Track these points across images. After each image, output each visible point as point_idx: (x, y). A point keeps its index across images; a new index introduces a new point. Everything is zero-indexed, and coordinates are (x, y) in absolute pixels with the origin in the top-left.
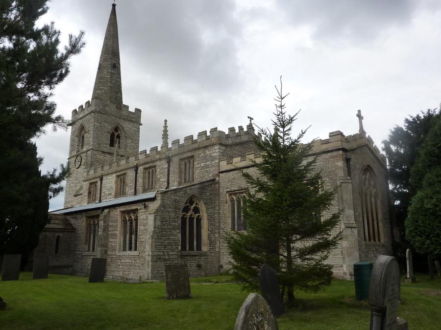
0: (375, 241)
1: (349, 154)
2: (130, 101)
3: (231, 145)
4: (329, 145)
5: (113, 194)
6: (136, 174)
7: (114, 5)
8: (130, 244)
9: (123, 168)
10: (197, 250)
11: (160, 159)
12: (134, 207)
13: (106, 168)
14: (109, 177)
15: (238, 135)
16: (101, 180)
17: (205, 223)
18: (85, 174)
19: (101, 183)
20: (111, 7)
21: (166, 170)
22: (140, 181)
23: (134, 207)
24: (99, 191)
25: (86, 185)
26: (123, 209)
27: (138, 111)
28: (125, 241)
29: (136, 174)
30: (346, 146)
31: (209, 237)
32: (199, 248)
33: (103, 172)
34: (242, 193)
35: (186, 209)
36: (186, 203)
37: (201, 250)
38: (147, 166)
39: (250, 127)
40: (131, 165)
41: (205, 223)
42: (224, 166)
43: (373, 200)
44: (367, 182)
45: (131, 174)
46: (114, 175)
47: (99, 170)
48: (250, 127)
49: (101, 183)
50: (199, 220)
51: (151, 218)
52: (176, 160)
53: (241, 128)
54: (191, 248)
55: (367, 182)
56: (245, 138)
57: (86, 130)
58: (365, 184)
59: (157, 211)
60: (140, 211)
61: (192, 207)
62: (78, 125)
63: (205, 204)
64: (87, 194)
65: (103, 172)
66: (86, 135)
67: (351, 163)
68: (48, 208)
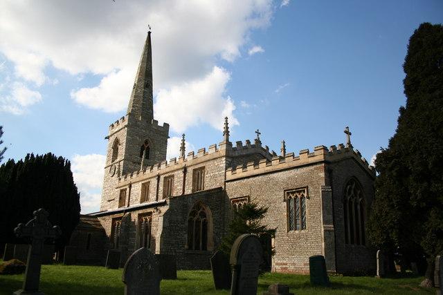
0: (358, 244)
1: (332, 166)
2: (161, 114)
3: (237, 157)
4: (315, 158)
5: (139, 199)
6: (158, 182)
7: (149, 33)
8: (146, 243)
9: (148, 177)
10: (203, 249)
11: (178, 170)
12: (149, 210)
13: (135, 176)
14: (136, 185)
15: (245, 148)
16: (130, 187)
17: (211, 228)
18: (117, 182)
19: (130, 189)
20: (147, 34)
21: (182, 179)
22: (161, 188)
23: (149, 210)
24: (127, 197)
25: (117, 192)
26: (141, 212)
27: (166, 126)
28: (141, 240)
29: (158, 182)
30: (329, 159)
31: (214, 239)
32: (205, 248)
33: (159, 171)
34: (243, 200)
35: (193, 214)
36: (194, 208)
37: (206, 250)
38: (167, 175)
39: (258, 141)
40: (179, 166)
41: (211, 226)
42: (230, 175)
43: (359, 207)
44: (352, 192)
45: (154, 181)
46: (140, 183)
47: (129, 177)
48: (258, 141)
49: (130, 189)
50: (205, 224)
51: (161, 219)
52: (190, 170)
53: (248, 142)
54: (197, 248)
55: (352, 192)
56: (251, 151)
57: (121, 142)
58: (350, 193)
59: (166, 214)
60: (153, 214)
61: (199, 212)
62: (112, 139)
63: (211, 209)
64: (118, 199)
65: (131, 180)
66: (119, 147)
67: (334, 174)
68: (79, 210)
